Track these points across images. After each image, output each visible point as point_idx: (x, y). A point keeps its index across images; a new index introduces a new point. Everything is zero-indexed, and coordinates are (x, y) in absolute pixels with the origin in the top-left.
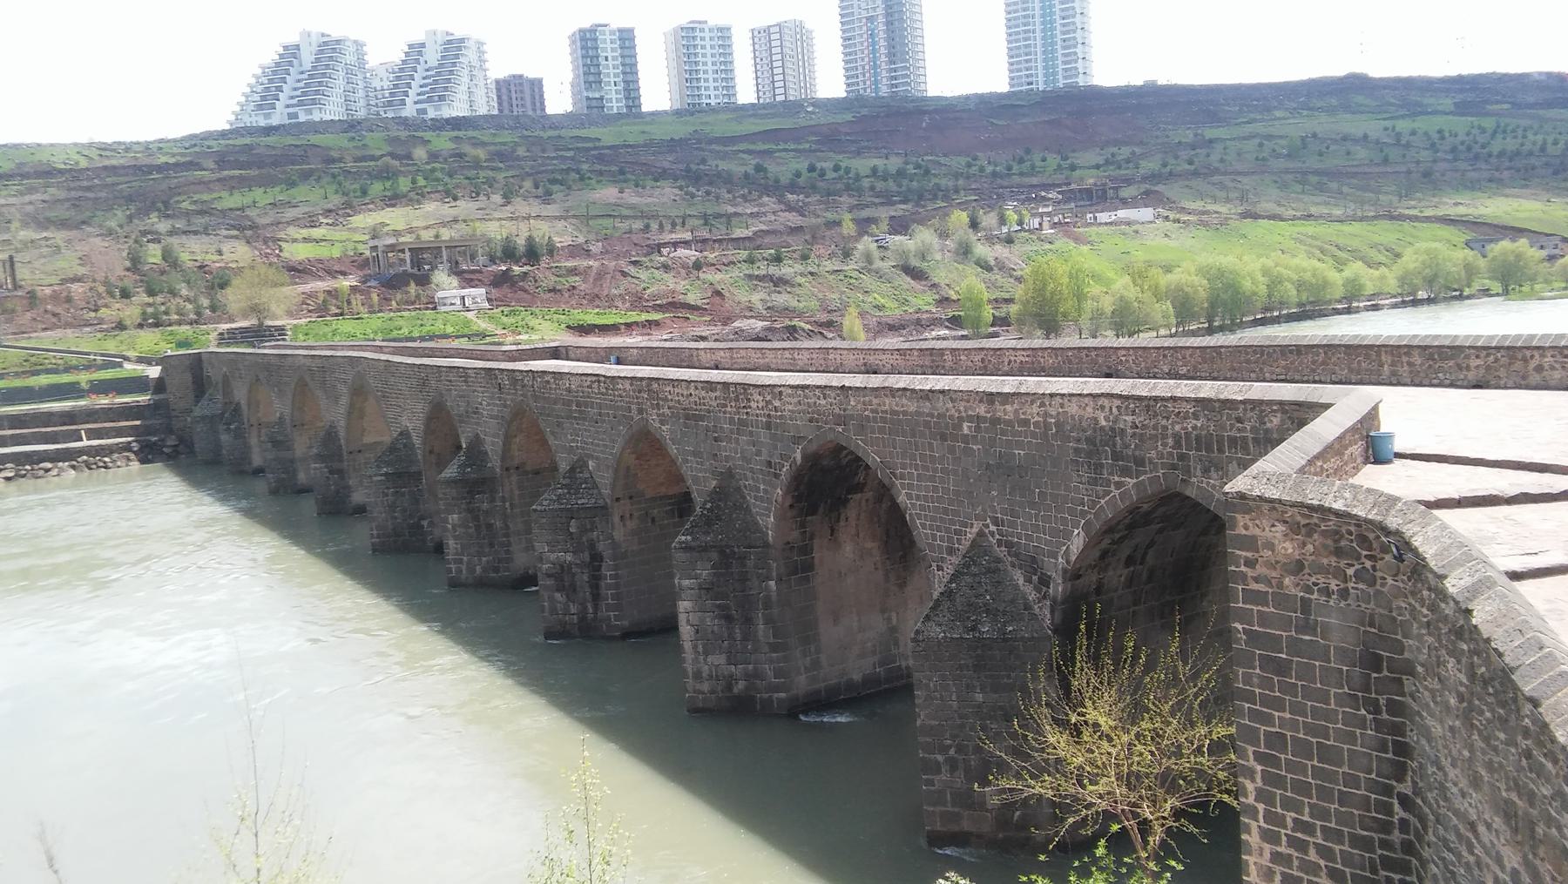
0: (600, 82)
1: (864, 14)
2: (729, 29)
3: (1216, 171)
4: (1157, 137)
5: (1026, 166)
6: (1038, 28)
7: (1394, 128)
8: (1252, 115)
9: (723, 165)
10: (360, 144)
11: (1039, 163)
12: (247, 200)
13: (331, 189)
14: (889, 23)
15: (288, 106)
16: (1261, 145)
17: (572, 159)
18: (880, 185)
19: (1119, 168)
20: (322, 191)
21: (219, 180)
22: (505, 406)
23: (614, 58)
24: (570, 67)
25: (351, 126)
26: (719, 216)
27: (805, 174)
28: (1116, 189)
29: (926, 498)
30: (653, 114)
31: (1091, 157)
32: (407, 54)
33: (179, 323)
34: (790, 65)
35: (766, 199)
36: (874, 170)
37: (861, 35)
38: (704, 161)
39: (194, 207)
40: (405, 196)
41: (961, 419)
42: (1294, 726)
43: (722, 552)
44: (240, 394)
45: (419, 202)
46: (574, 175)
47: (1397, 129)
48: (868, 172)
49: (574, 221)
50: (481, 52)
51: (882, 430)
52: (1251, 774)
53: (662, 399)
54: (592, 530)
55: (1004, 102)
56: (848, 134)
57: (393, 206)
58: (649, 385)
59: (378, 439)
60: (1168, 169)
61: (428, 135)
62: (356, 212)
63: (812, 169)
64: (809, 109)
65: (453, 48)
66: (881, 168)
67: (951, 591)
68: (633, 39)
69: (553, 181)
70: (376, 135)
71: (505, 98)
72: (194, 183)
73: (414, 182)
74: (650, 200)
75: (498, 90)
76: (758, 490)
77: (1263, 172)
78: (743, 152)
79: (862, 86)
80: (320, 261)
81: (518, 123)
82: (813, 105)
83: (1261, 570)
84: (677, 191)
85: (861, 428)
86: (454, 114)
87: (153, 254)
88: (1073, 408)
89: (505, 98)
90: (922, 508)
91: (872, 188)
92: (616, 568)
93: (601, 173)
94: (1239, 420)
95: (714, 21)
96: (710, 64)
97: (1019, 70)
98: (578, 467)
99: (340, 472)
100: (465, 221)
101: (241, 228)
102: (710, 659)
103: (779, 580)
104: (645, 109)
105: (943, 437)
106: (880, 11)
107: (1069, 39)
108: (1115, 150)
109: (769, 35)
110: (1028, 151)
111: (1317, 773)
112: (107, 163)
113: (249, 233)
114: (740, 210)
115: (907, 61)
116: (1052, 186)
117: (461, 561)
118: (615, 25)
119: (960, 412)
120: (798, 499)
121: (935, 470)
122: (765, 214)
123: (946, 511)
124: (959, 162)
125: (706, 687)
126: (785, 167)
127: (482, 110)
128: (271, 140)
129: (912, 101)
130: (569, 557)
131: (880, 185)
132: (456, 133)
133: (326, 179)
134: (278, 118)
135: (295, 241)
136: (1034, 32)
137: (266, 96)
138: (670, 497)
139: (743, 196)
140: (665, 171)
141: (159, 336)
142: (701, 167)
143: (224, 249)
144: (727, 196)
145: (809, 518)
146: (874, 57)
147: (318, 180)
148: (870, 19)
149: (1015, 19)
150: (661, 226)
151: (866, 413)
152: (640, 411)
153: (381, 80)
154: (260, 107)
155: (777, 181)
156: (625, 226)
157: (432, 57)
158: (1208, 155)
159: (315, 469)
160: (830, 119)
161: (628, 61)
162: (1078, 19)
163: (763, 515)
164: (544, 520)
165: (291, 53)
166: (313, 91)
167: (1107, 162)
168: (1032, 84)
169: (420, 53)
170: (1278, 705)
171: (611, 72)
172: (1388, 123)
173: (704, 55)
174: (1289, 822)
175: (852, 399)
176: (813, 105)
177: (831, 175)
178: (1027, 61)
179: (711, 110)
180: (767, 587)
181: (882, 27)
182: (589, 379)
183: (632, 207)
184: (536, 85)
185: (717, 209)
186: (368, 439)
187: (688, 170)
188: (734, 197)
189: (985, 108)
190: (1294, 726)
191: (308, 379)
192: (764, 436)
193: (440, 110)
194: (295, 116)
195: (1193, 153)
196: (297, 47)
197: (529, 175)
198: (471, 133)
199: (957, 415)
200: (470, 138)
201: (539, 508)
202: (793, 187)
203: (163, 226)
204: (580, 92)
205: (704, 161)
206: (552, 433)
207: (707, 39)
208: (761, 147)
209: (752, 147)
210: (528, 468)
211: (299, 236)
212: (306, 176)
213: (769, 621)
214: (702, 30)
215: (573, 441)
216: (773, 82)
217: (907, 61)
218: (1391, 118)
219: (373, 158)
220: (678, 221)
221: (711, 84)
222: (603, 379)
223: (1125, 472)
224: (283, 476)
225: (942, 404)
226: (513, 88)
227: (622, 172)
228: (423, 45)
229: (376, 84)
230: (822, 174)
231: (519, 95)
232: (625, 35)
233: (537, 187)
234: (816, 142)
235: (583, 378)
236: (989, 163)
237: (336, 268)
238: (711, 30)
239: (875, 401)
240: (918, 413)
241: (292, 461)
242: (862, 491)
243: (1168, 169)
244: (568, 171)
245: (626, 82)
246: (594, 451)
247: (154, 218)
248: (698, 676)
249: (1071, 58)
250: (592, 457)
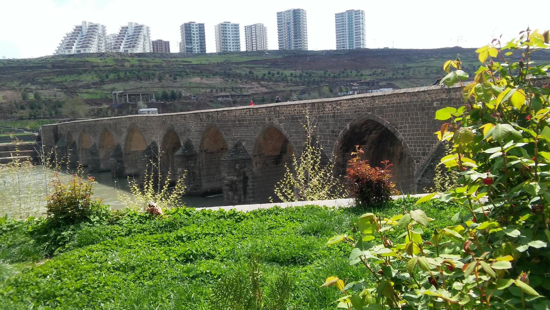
0: (192, 42)
1: (286, 21)
2: (238, 25)
3: (411, 78)
4: (390, 66)
5: (345, 74)
6: (347, 28)
7: (472, 65)
8: (422, 60)
9: (238, 71)
10: (104, 61)
11: (350, 74)
12: (64, 79)
13: (95, 76)
14: (295, 25)
15: (77, 48)
16: (426, 69)
17: (182, 68)
18: (294, 79)
19: (378, 75)
20: (91, 77)
21: (52, 72)
22: (203, 126)
23: (197, 34)
24: (181, 37)
25: (100, 55)
26: (237, 88)
27: (267, 75)
28: (378, 82)
29: (413, 135)
30: (211, 54)
31: (367, 72)
32: (121, 31)
33: (44, 118)
34: (258, 39)
35: (253, 83)
36: (292, 74)
37: (285, 29)
38: (230, 69)
39: (43, 81)
40: (123, 79)
41: (433, 101)
44: (75, 138)
45: (128, 81)
46: (184, 73)
47: (474, 65)
48: (289, 75)
49: (185, 88)
50: (148, 31)
51: (390, 111)
53: (281, 114)
54: (244, 168)
55: (336, 53)
56: (280, 62)
57: (118, 82)
58: (274, 109)
59: (136, 149)
60: (395, 77)
61: (129, 59)
62: (104, 84)
63: (269, 73)
64: (267, 53)
65: (138, 29)
66: (294, 74)
67: (432, 166)
68: (204, 27)
69: (177, 75)
70: (109, 58)
71: (155, 48)
72: (43, 73)
73: (126, 74)
74: (212, 82)
75: (153, 45)
76: (327, 142)
77: (428, 78)
78: (244, 67)
79: (285, 47)
80: (93, 100)
81: (162, 56)
82: (268, 52)
84: (222, 80)
86: (138, 52)
87: (31, 96)
89: (155, 48)
90: (410, 139)
91: (291, 80)
92: (253, 182)
93: (194, 73)
95: (233, 22)
96: (231, 37)
97: (340, 43)
98: (237, 146)
99: (121, 162)
100: (145, 88)
101: (62, 89)
104: (207, 52)
105: (423, 109)
106: (292, 20)
107: (358, 32)
108: (376, 70)
109: (251, 28)
110: (345, 69)
112: (10, 65)
113: (65, 90)
114: (244, 86)
115: (301, 38)
116: (355, 81)
118: (197, 22)
119: (432, 98)
120: (344, 145)
121: (419, 123)
122: (254, 88)
123: (423, 139)
124: (322, 72)
126: (260, 72)
127: (148, 51)
128: (71, 59)
129: (303, 52)
130: (235, 178)
131: (294, 79)
132: (139, 58)
133: (92, 73)
134: (74, 51)
135: (83, 93)
136: (346, 29)
137: (68, 44)
138: (274, 156)
139: (245, 82)
140: (217, 72)
141: (37, 122)
142: (230, 72)
144: (240, 81)
145: (346, 154)
146: (289, 37)
147: (90, 73)
148: (288, 23)
149: (339, 25)
150: (217, 91)
151: (384, 105)
152: (270, 119)
153: (111, 40)
154: (67, 48)
155: (257, 77)
156: (204, 90)
157: (130, 32)
158: (408, 72)
159: (111, 160)
160: (274, 57)
161: (202, 35)
162: (361, 25)
163: (328, 152)
164: (226, 164)
165: (79, 29)
166: (86, 42)
167: (374, 74)
168: (344, 47)
169: (126, 31)
171: (196, 38)
172: (471, 63)
175: (377, 101)
176: (268, 52)
177: (276, 76)
178: (343, 40)
179: (232, 53)
181: (292, 26)
182: (245, 110)
183: (206, 84)
184: (167, 44)
185: (236, 86)
186: (133, 149)
187: (225, 72)
188: (243, 82)
189: (329, 54)
191: (108, 128)
192: (331, 121)
193: (133, 51)
194: (80, 51)
195: (403, 71)
196: (81, 27)
197: (168, 73)
198: (145, 59)
199: (431, 100)
200: (144, 60)
201: (224, 159)
202: (263, 79)
203: (33, 87)
204: (184, 46)
205: (230, 69)
206: (225, 134)
207: (230, 28)
208: (250, 66)
209: (247, 66)
210: (209, 151)
211: (83, 91)
212: (85, 71)
214: (228, 25)
215: (235, 135)
216: (252, 45)
217: (301, 38)
218: (472, 61)
219: (109, 66)
220: (223, 89)
221: (231, 44)
222: (252, 109)
224: (95, 166)
225: (422, 97)
226: (158, 45)
227: (201, 73)
228: (127, 28)
229: (109, 41)
230: (273, 75)
231: (160, 47)
232: (201, 26)
233: (171, 77)
234: (270, 65)
235: (242, 110)
236: (332, 73)
237: (99, 102)
238: (232, 25)
239: (388, 100)
240: (411, 102)
241: (98, 160)
242: (365, 144)
244: (182, 71)
245: (201, 42)
246: (246, 138)
247: (29, 85)
249: (358, 39)
250: (244, 141)
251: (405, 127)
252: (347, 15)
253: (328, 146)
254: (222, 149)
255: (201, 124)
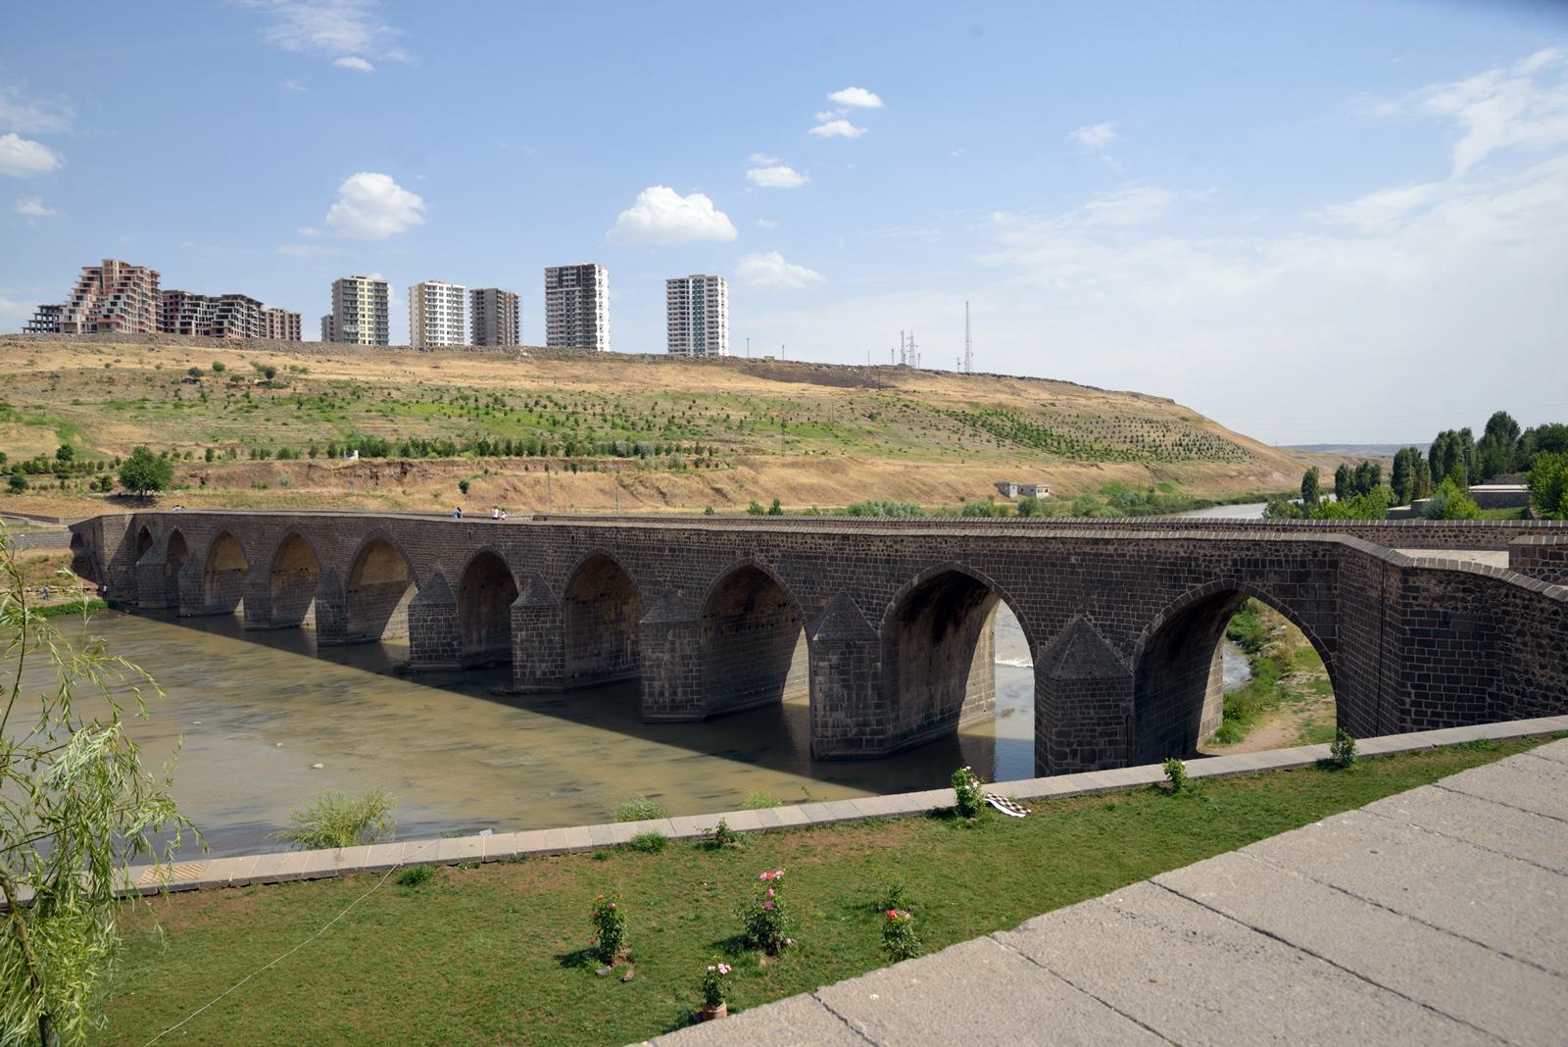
29: (1034, 602)
42: (1435, 669)
43: (848, 645)
52: (1409, 695)
64: (525, 354)
83: (1420, 601)
85: (975, 563)
88: (1162, 547)
90: (1030, 608)
94: (1277, 551)
102: (834, 714)
103: (883, 663)
105: (1054, 565)
111: (1445, 689)
117: (525, 667)
125: (830, 733)
138: (732, 617)
143: (533, 403)
152: (747, 554)
170: (1428, 661)
173: (442, 301)
174: (1429, 713)
180: (876, 667)
186: (365, 582)
190: (1435, 669)
213: (875, 688)
221: (446, 329)
223: (1197, 580)
225: (1053, 546)
239: (993, 544)
240: (1032, 552)
243: (409, 468)
248: (825, 725)
251: (1023, 589)
252: (691, 284)
253: (874, 610)
254: (602, 595)
255: (571, 548)
